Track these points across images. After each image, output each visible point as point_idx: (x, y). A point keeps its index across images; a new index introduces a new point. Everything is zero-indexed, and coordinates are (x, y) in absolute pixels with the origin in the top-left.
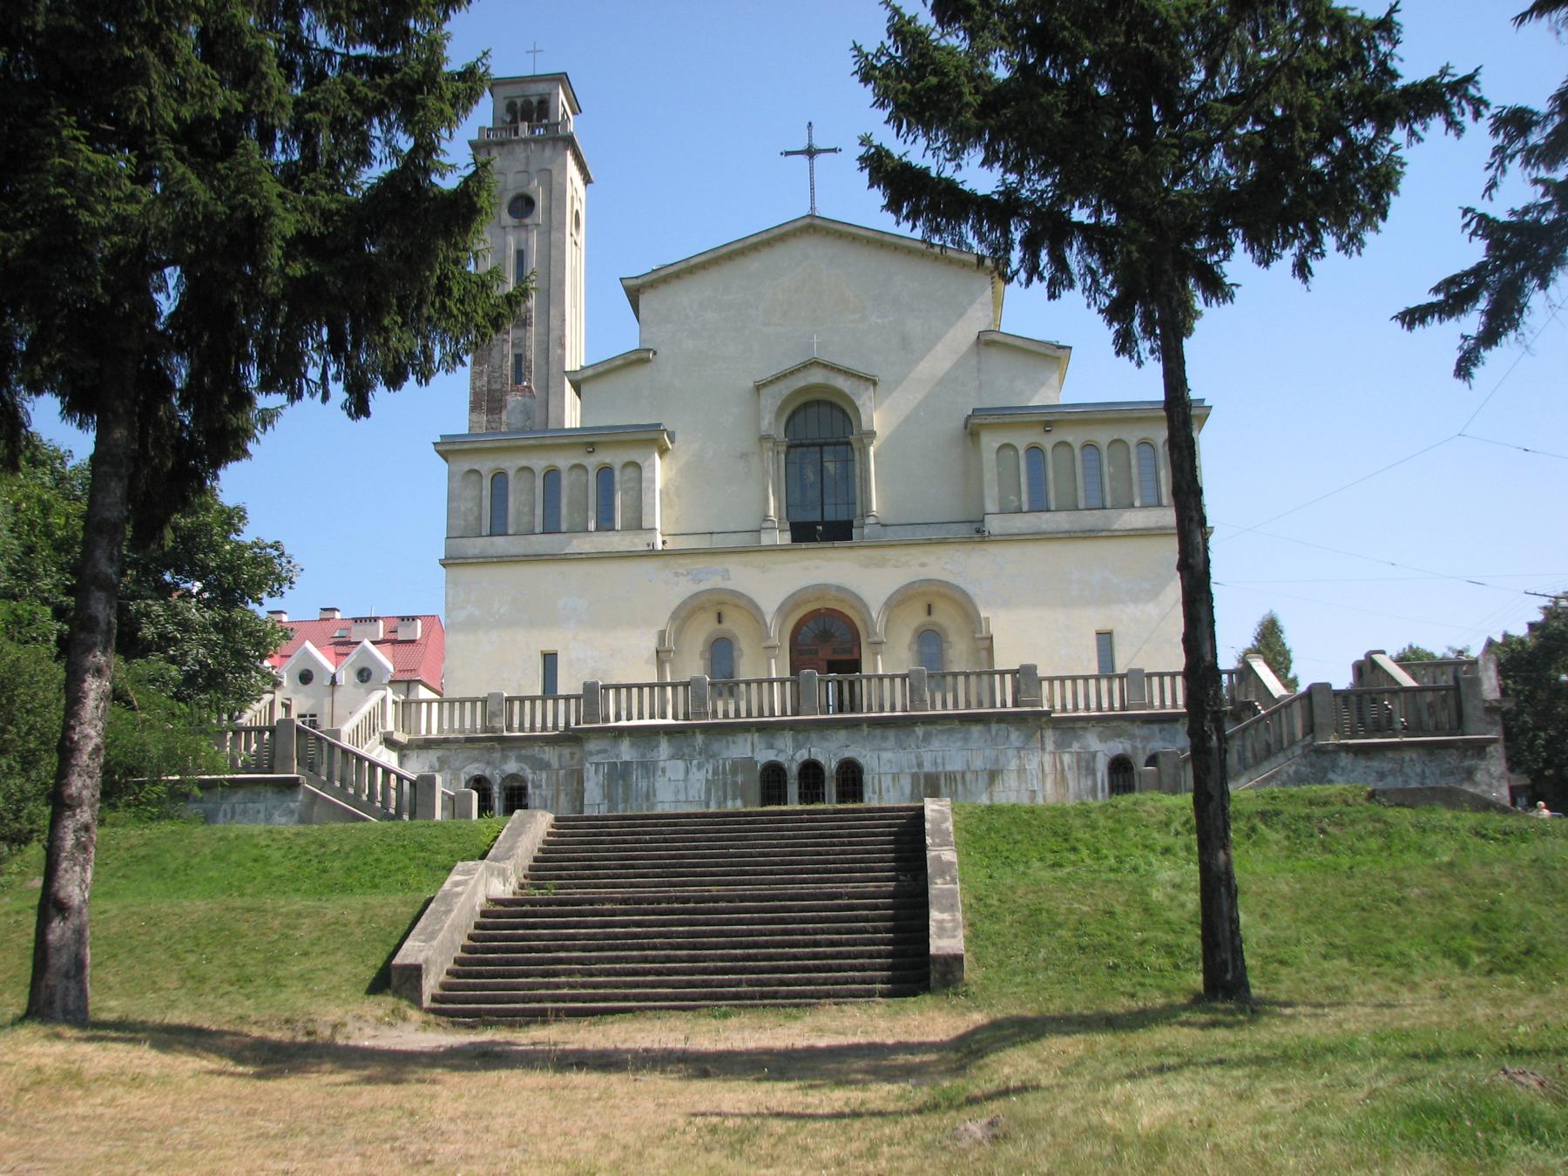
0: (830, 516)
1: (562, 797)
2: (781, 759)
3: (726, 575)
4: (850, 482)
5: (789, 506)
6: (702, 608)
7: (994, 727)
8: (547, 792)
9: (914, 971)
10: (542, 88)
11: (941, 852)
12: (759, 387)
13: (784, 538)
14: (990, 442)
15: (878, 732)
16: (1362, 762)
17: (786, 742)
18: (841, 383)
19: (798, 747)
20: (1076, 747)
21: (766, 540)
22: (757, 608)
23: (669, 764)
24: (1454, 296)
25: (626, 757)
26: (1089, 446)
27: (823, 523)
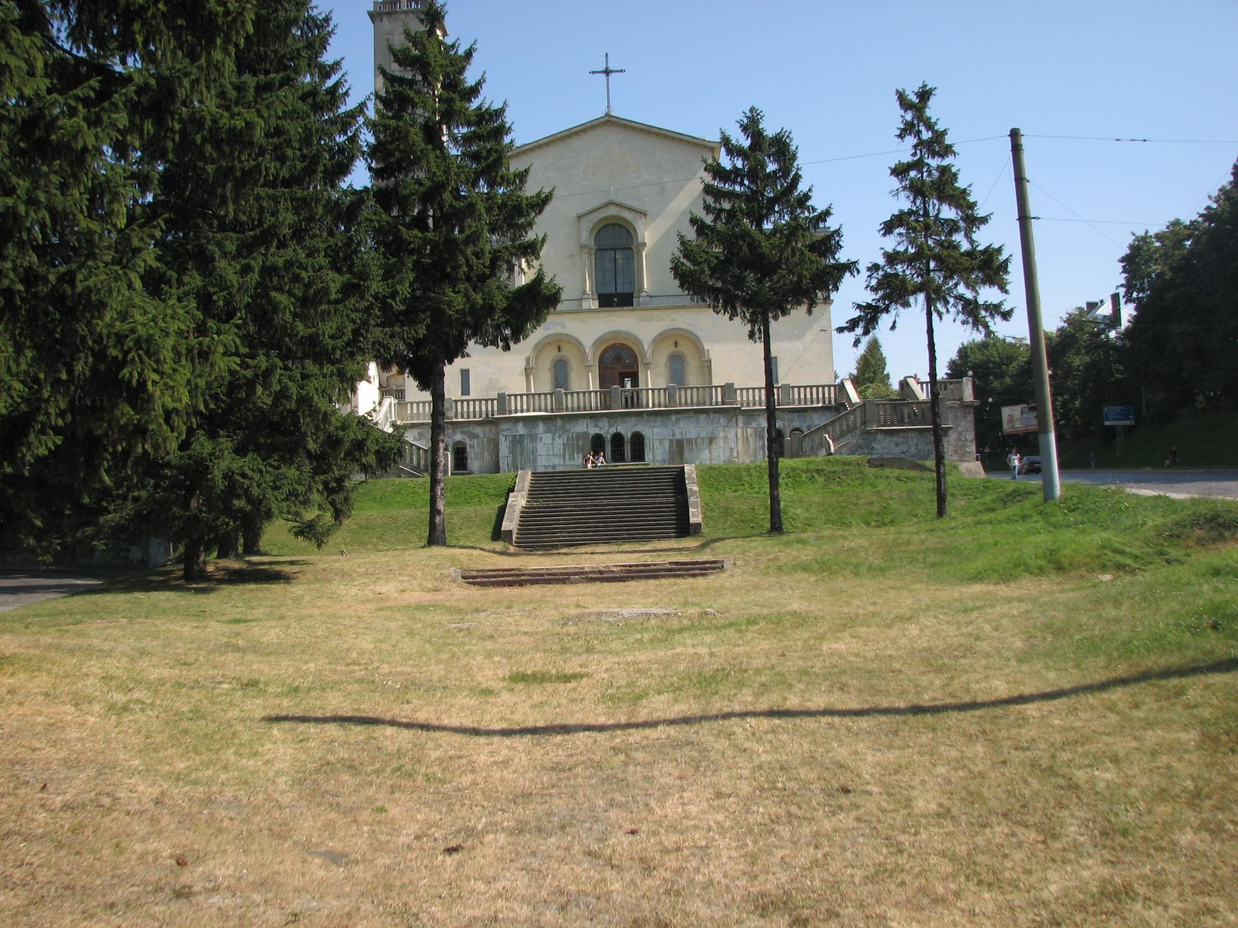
0: (620, 290)
1: (486, 453)
2: (602, 432)
3: (563, 325)
4: (631, 269)
5: (598, 283)
6: (550, 344)
7: (712, 416)
8: (477, 450)
9: (684, 528)
11: (692, 487)
12: (579, 217)
13: (594, 305)
15: (652, 418)
18: (627, 215)
19: (610, 426)
20: (754, 425)
21: (585, 305)
22: (581, 344)
23: (544, 436)
24: (853, 324)
25: (521, 432)
27: (617, 297)
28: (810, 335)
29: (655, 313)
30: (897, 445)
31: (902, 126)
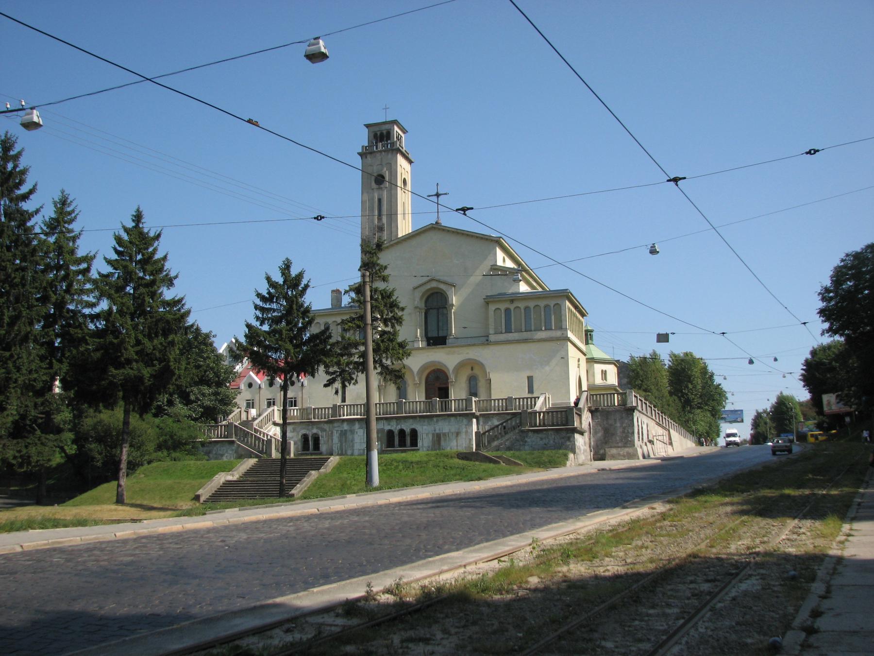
2: (392, 429)
8: (325, 439)
10: (387, 127)
12: (415, 288)
14: (492, 307)
16: (536, 435)
17: (394, 423)
18: (442, 286)
19: (397, 425)
20: (490, 423)
26: (527, 308)
28: (554, 362)
29: (456, 349)
30: (542, 439)
31: (264, 290)
